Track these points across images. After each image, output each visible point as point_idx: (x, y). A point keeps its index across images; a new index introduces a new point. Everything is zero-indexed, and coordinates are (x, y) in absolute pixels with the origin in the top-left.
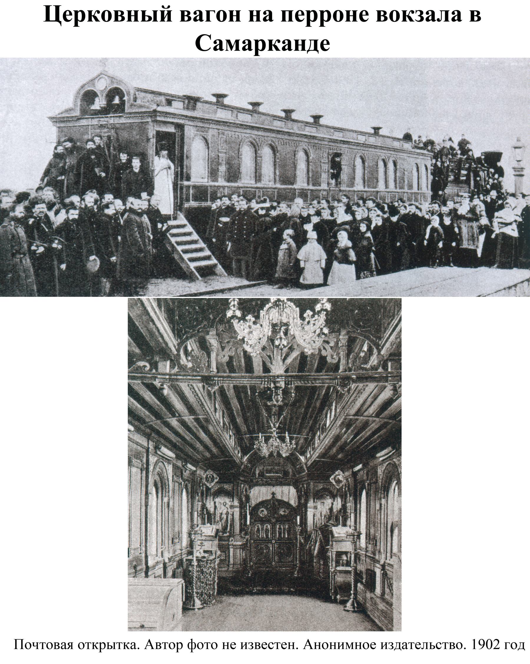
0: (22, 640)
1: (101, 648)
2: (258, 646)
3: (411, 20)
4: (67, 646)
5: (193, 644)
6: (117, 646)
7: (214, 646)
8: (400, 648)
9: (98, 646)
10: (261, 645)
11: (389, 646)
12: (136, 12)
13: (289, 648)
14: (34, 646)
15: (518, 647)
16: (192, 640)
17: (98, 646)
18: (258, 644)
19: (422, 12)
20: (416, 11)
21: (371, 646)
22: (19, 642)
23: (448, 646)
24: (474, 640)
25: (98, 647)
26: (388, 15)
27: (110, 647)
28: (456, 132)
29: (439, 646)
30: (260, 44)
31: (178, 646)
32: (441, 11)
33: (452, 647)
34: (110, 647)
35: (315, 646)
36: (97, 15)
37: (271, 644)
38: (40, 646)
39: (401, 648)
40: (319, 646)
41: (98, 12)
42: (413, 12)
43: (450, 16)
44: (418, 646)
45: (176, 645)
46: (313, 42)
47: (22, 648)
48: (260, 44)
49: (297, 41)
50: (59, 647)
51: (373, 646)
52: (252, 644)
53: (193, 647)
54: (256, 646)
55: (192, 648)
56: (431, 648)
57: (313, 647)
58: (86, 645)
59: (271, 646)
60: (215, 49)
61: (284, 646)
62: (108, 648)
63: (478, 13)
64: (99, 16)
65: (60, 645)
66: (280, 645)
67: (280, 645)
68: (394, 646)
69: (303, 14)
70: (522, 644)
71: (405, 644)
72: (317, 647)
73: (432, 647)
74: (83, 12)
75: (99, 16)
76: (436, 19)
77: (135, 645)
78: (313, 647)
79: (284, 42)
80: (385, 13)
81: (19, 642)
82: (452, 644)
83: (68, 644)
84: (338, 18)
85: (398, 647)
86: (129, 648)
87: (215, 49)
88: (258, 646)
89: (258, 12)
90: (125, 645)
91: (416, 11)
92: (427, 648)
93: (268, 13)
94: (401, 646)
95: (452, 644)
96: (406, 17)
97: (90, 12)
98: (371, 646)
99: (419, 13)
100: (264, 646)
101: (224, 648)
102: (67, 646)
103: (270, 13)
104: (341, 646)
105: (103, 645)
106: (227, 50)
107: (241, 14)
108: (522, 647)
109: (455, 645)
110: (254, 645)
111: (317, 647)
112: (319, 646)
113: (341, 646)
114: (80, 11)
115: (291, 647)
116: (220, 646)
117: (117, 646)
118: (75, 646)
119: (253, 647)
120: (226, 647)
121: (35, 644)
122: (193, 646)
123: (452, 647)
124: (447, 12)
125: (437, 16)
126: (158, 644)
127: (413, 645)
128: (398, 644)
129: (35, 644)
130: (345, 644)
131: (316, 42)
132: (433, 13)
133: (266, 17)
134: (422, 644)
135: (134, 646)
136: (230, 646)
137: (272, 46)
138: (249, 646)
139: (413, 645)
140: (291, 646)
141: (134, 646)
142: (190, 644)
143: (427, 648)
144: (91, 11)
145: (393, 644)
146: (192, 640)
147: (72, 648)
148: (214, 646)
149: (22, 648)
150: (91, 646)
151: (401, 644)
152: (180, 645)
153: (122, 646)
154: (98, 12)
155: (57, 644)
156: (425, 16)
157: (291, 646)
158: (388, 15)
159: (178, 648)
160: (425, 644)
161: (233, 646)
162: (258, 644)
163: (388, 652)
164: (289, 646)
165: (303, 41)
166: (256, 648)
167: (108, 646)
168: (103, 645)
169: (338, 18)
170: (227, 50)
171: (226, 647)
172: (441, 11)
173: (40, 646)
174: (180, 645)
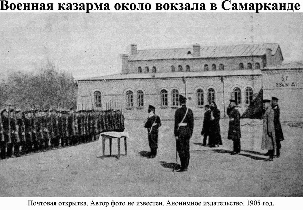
0: (32, 201)
1: (69, 205)
2: (144, 204)
3: (176, 9)
4: (53, 204)
5: (114, 203)
6: (77, 204)
7: (124, 204)
8: (212, 205)
9: (68, 204)
10: (146, 204)
11: (207, 204)
12: (29, 4)
13: (160, 205)
14: (37, 204)
15: (269, 204)
16: (113, 201)
17: (68, 204)
18: (144, 203)
19: (182, 4)
20: (179, 4)
21: (199, 204)
22: (30, 202)
23: (236, 204)
24: (248, 201)
25: (68, 204)
26: (162, 6)
27: (74, 204)
28: (63, 179)
29: (231, 204)
30: (259, 6)
31: (106, 204)
32: (194, 4)
33: (238, 204)
34: (74, 204)
35: (172, 204)
36: (127, 6)
37: (151, 203)
38: (40, 204)
39: (213, 205)
40: (174, 204)
41: (128, 4)
42: (177, 4)
43: (199, 7)
44: (221, 204)
45: (105, 203)
46: (290, 5)
47: (32, 205)
48: (259, 6)
49: (281, 4)
50: (49, 204)
51: (200, 204)
52: (142, 203)
53: (114, 204)
54: (144, 204)
55: (113, 205)
56: (227, 205)
57: (171, 204)
58: (62, 204)
59: (151, 204)
60: (233, 9)
61: (157, 204)
62: (73, 205)
63: (215, 5)
64: (128, 7)
65: (50, 204)
66: (155, 204)
67: (155, 204)
68: (210, 204)
69: (21, 5)
70: (271, 203)
71: (215, 203)
72: (173, 204)
73: (228, 204)
74: (261, 4)
75: (128, 7)
76: (191, 8)
77: (86, 203)
78: (171, 204)
79: (273, 5)
80: (161, 5)
81: (30, 202)
82: (238, 203)
83: (54, 203)
84: (166, 8)
85: (212, 204)
86: (83, 204)
87: (233, 9)
88: (144, 204)
89: (37, 4)
90: (81, 204)
91: (74, 4)
92: (225, 205)
93: (202, 5)
94: (213, 204)
95: (238, 203)
96: (173, 7)
97: (265, 4)
98: (199, 204)
99: (180, 5)
100: (148, 204)
101: (128, 205)
102: (53, 204)
103: (204, 5)
104: (184, 204)
105: (70, 204)
106: (240, 9)
107: (53, 5)
108: (271, 204)
109: (239, 204)
110: (143, 204)
111: (173, 204)
112: (174, 204)
113: (184, 204)
114: (260, 4)
115: (161, 204)
116: (127, 204)
117: (77, 204)
118: (57, 204)
119: (142, 204)
120: (129, 204)
121: (38, 203)
122: (113, 204)
123: (238, 204)
124: (197, 4)
125: (191, 7)
126: (97, 203)
127: (219, 204)
128: (212, 203)
129: (38, 203)
130: (186, 203)
131: (292, 4)
132: (189, 5)
133: (41, 7)
134: (223, 203)
135: (85, 204)
136: (130, 204)
137: (266, 7)
138: (140, 204)
139: (219, 204)
140: (161, 204)
141: (85, 204)
142: (112, 203)
143: (225, 205)
144: (266, 4)
145: (209, 203)
146: (113, 201)
147: (56, 205)
148: (124, 204)
149: (32, 205)
150: (65, 204)
151: (213, 203)
152: (107, 204)
153: (80, 204)
154: (128, 4)
155: (48, 203)
156: (184, 7)
157: (161, 204)
158: (162, 6)
159: (106, 205)
160: (225, 203)
161: (133, 204)
162: (144, 203)
163: (207, 207)
164: (160, 204)
165: (285, 4)
166: (144, 205)
167: (73, 204)
168: (70, 204)
169: (166, 8)
170: (240, 9)
171: (129, 204)
172: (194, 4)
173: (40, 204)
174: (107, 204)
